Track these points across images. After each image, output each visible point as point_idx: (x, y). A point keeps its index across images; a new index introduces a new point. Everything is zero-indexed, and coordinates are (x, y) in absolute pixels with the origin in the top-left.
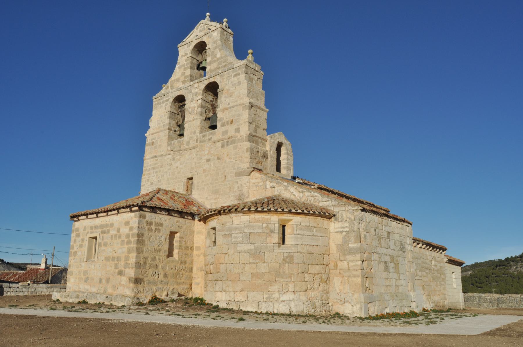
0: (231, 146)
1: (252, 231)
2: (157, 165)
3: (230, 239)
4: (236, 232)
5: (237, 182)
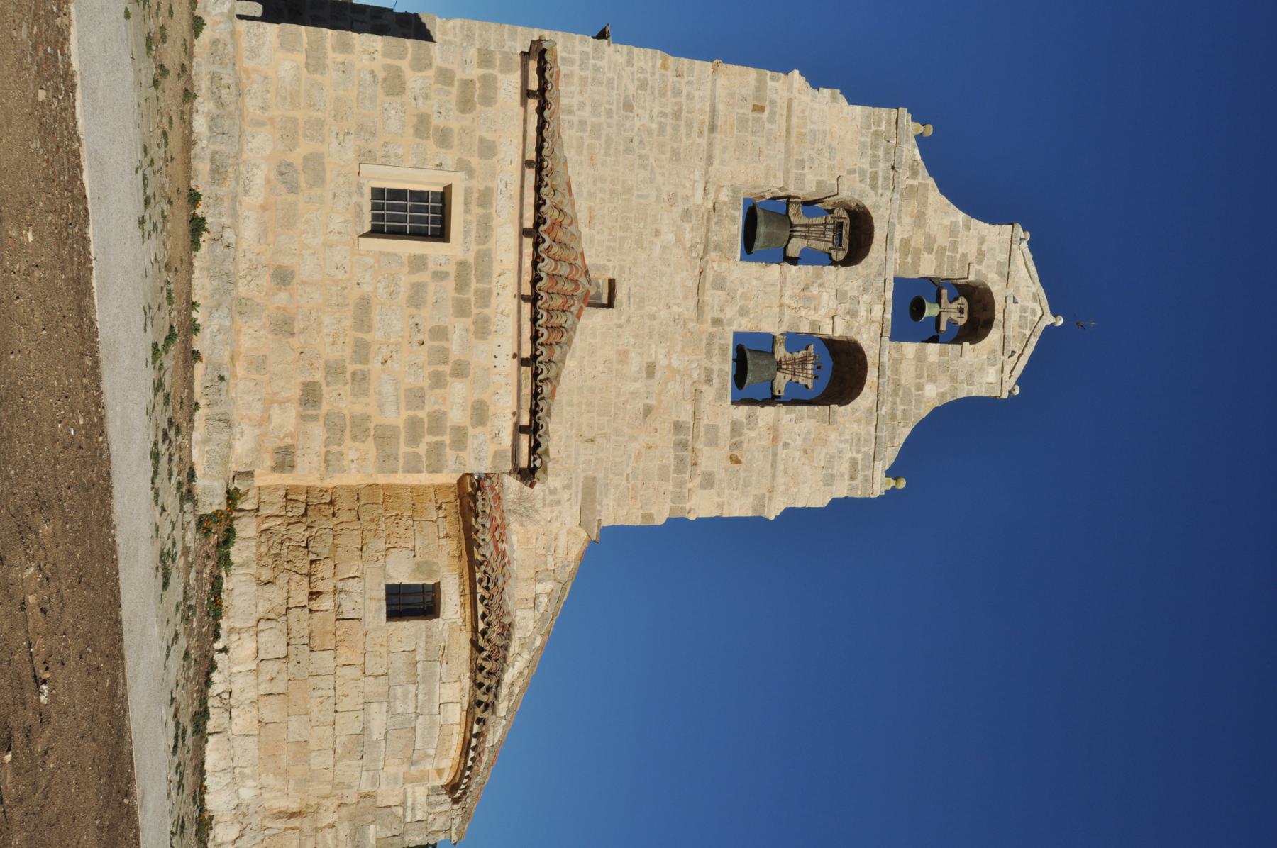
0: (670, 456)
1: (419, 731)
2: (683, 130)
3: (403, 678)
4: (420, 697)
5: (567, 487)
